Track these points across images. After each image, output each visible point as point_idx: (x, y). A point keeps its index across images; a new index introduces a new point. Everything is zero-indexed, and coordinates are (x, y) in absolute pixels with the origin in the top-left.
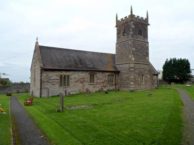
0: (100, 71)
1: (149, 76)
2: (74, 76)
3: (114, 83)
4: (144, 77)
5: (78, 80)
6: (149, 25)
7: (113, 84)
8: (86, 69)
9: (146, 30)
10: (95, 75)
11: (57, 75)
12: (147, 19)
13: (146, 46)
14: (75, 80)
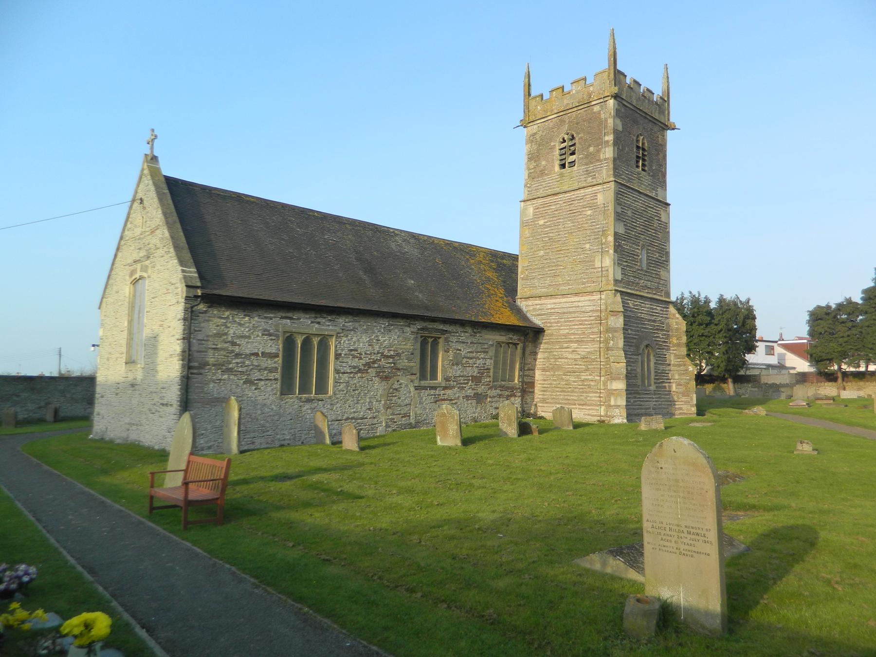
0: (462, 323)
2: (354, 343)
5: (368, 365)
7: (512, 388)
8: (405, 312)
9: (660, 149)
10: (441, 341)
11: (270, 335)
12: (664, 104)
14: (355, 362)
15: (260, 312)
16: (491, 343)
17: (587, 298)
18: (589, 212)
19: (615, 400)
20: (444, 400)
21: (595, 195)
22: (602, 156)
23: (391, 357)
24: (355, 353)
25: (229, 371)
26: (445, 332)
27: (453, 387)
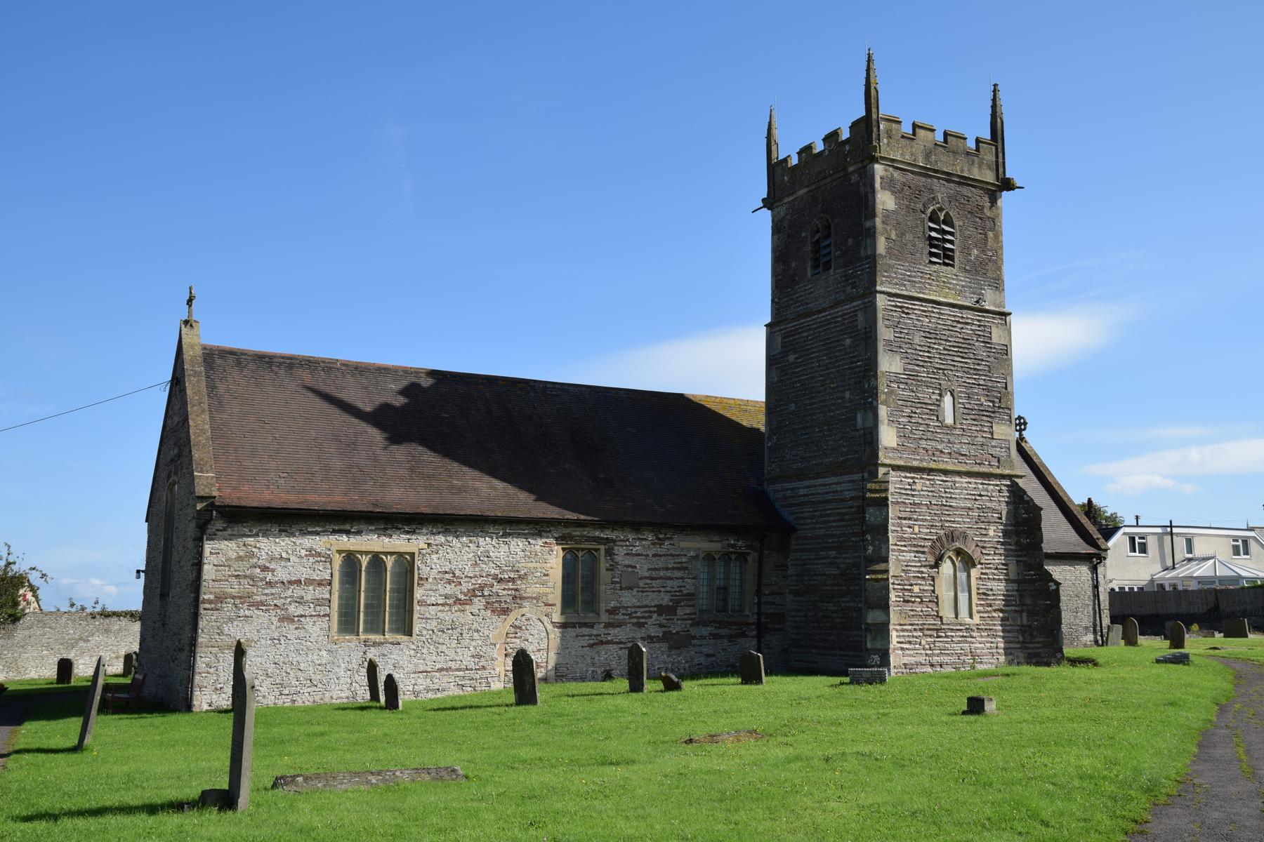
5: (472, 593)
6: (1008, 185)
13: (987, 342)
14: (449, 589)
15: (302, 526)
16: (692, 554)
18: (848, 341)
19: (873, 639)
20: (608, 642)
23: (513, 580)
25: (258, 605)
27: (625, 624)
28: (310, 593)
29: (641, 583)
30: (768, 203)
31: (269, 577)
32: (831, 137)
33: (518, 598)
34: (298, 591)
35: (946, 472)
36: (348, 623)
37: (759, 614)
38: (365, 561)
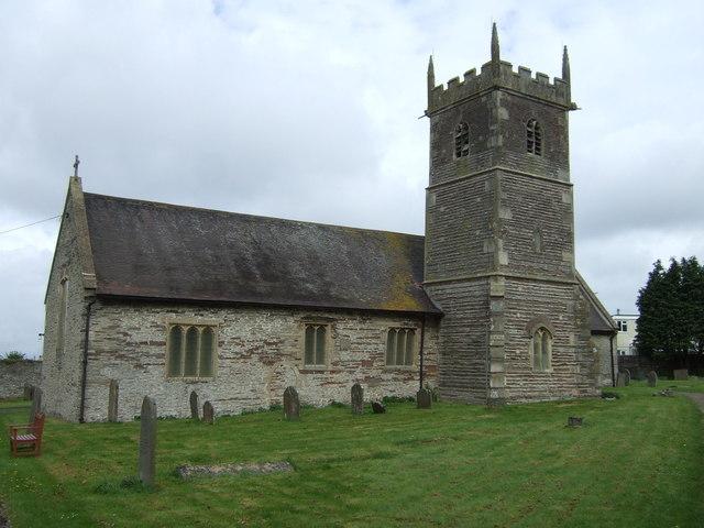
1: (572, 339)
2: (237, 330)
3: (415, 367)
4: (550, 343)
5: (251, 351)
6: (573, 107)
7: (410, 372)
8: (290, 303)
9: (561, 132)
10: (328, 329)
11: (158, 326)
14: (238, 349)
16: (383, 328)
17: (476, 283)
21: (483, 182)
22: (489, 145)
23: (274, 343)
24: (238, 341)
25: (121, 357)
26: (333, 320)
28: (155, 350)
29: (353, 346)
30: (427, 114)
31: (128, 339)
32: (470, 74)
33: (279, 355)
34: (144, 349)
35: (535, 280)
36: (174, 371)
37: (421, 366)
38: (201, 330)
